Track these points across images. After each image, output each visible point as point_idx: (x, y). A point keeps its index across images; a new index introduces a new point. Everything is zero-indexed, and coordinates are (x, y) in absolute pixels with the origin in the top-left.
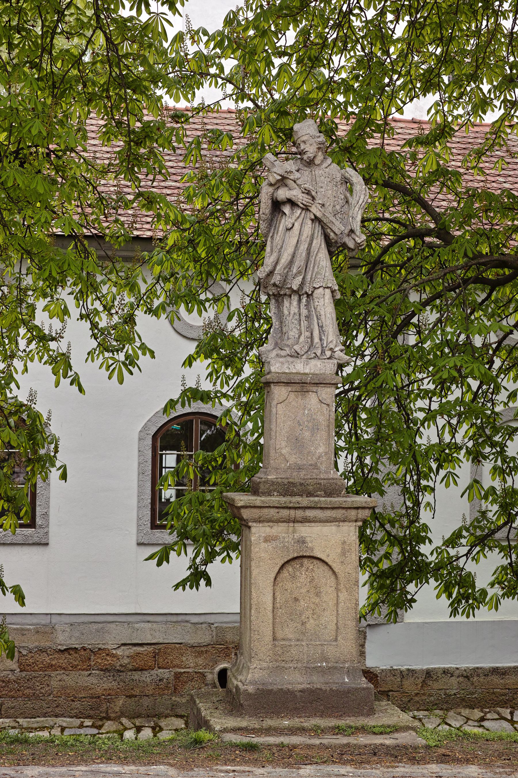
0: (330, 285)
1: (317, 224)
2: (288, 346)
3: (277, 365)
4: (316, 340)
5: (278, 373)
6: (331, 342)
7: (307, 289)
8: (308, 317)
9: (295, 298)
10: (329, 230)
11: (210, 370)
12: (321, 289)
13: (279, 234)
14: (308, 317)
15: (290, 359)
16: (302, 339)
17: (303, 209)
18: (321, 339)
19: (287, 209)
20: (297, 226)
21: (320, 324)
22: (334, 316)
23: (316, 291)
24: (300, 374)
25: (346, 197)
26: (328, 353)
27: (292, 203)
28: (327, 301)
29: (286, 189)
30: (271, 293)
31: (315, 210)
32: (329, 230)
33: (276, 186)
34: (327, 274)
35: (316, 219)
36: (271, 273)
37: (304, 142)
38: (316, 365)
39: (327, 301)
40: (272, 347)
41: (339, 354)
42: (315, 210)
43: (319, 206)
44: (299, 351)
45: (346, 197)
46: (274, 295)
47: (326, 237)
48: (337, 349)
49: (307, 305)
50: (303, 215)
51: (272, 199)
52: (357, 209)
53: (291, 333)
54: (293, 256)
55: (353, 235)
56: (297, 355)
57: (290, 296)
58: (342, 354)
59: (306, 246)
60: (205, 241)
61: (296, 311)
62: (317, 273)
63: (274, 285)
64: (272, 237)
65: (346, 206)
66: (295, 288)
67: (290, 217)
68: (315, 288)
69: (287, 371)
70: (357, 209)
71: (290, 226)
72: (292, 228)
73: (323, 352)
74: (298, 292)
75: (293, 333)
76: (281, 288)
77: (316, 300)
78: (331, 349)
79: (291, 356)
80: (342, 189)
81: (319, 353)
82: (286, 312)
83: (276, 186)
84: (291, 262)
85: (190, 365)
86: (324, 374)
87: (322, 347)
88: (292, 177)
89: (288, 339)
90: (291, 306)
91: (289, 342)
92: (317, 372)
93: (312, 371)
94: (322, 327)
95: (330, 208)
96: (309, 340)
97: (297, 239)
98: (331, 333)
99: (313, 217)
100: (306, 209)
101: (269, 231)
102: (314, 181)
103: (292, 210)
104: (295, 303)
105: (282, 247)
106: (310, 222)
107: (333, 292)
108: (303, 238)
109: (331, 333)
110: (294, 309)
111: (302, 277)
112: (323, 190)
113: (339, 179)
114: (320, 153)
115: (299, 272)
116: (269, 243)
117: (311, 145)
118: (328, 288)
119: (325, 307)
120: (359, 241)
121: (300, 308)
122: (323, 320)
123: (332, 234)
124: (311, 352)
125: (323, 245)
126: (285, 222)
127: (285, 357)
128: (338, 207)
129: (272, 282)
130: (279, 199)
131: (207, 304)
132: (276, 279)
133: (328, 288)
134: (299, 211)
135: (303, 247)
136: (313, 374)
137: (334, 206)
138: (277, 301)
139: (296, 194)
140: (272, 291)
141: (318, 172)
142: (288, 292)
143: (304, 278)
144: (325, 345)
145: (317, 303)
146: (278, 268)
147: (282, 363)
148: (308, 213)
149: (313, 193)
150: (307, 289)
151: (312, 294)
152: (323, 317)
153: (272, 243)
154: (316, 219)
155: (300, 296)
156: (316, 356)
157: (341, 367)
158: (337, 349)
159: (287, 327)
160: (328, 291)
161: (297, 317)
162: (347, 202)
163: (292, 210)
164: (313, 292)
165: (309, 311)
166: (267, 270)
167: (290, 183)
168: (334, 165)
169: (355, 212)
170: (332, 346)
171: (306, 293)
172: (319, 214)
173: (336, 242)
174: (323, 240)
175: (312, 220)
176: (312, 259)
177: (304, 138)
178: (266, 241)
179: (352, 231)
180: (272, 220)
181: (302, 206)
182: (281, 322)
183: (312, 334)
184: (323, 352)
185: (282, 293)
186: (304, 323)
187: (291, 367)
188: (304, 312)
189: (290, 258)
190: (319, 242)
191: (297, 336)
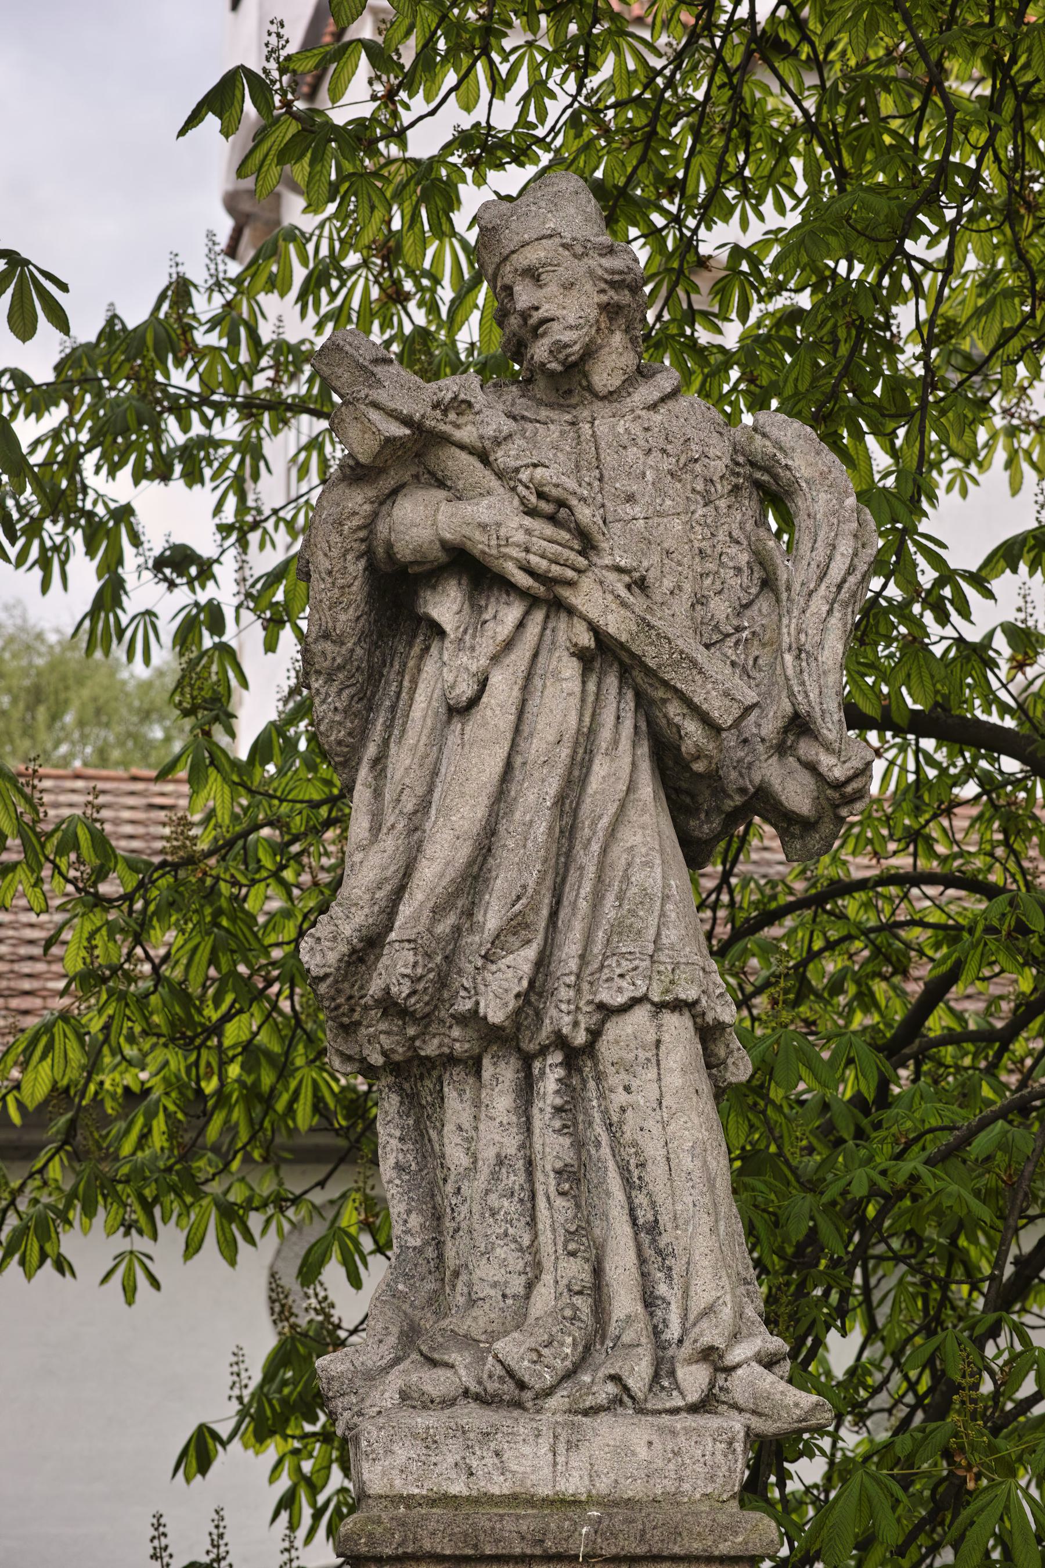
0: (690, 993)
1: (612, 681)
2: (468, 1341)
3: (402, 1453)
4: (624, 1302)
5: (408, 1501)
6: (709, 1311)
7: (562, 1017)
8: (574, 1177)
9: (501, 1075)
10: (674, 709)
11: (284, 1482)
12: (641, 1015)
13: (411, 738)
14: (574, 1177)
15: (474, 1417)
16: (543, 1299)
17: (532, 601)
18: (650, 1301)
19: (445, 606)
20: (503, 686)
21: (644, 1216)
22: (720, 1166)
23: (618, 1030)
24: (530, 1501)
25: (761, 560)
26: (694, 1379)
27: (471, 569)
28: (674, 1080)
29: (442, 494)
30: (376, 1059)
31: (597, 601)
32: (674, 709)
33: (387, 483)
34: (671, 935)
35: (603, 654)
36: (369, 947)
37: (533, 274)
38: (624, 1450)
39: (674, 1080)
40: (385, 1352)
41: (752, 1381)
42: (597, 601)
43: (618, 584)
44: (524, 1368)
45: (761, 560)
46: (394, 1067)
47: (666, 756)
48: (739, 1353)
49: (570, 1110)
50: (533, 629)
51: (369, 553)
52: (818, 605)
53: (486, 1272)
54: (486, 844)
55: (806, 748)
56: (513, 1394)
57: (475, 1066)
58: (773, 1384)
59: (553, 787)
60: (214, 951)
61: (511, 1144)
62: (619, 929)
63: (388, 1006)
64: (379, 762)
65: (764, 604)
66: (496, 1013)
67: (467, 643)
68: (607, 1011)
69: (458, 1488)
70: (818, 605)
71: (465, 689)
72: (474, 702)
73: (663, 1371)
74: (509, 1039)
75: (494, 1270)
76: (425, 1020)
77: (615, 1080)
78: (709, 1355)
79: (485, 1400)
80: (739, 516)
81: (639, 1373)
82: (456, 1156)
83: (387, 483)
84: (474, 878)
85: (204, 1465)
86: (673, 1498)
87: (660, 1344)
88: (466, 434)
89: (472, 1302)
90: (482, 1121)
91: (476, 1323)
92: (633, 1490)
93: (603, 1486)
94: (654, 1228)
95: (681, 605)
96: (584, 1304)
97: (501, 752)
98: (704, 1265)
99: (586, 639)
100: (549, 599)
101: (362, 734)
102: (591, 462)
103: (477, 609)
104: (502, 1102)
105: (424, 805)
106: (571, 668)
107: (708, 1034)
108: (536, 747)
109: (704, 1265)
110: (498, 1136)
111: (531, 953)
112: (637, 510)
113: (719, 467)
114: (618, 339)
115: (516, 927)
116: (361, 795)
117: (568, 286)
118: (678, 1006)
119: (667, 1114)
120: (839, 773)
121: (528, 1128)
122: (660, 1188)
123: (692, 727)
124: (588, 1369)
125: (647, 789)
126: (440, 674)
127: (448, 1403)
128: (720, 608)
129: (375, 987)
130: (404, 551)
131: (255, 1221)
132: (395, 970)
133: (678, 1006)
134: (512, 613)
135: (536, 794)
136: (610, 1503)
137: (700, 600)
138: (411, 1101)
139: (487, 515)
140: (380, 1040)
141: (608, 425)
142: (459, 1040)
143: (542, 962)
144: (674, 1331)
145: (620, 1098)
146: (405, 911)
147: (430, 1441)
148: (562, 623)
149: (585, 514)
150: (562, 1017)
151: (590, 1049)
152: (656, 1172)
153: (378, 794)
154: (603, 654)
155: (527, 1060)
156: (624, 1398)
157: (770, 1454)
158: (739, 1353)
159: (463, 1240)
160: (678, 1028)
161: (515, 1180)
162: (768, 583)
163: (477, 609)
164: (595, 1034)
165: (579, 1145)
166: (347, 930)
167: (461, 465)
168: (690, 399)
169: (811, 622)
170: (711, 1335)
171: (561, 1041)
172: (617, 624)
173: (714, 778)
174: (645, 767)
175: (585, 658)
176: (587, 859)
177: (532, 256)
178: (348, 789)
179: (799, 725)
180: (374, 677)
181: (523, 580)
182: (437, 1217)
183: (598, 1272)
184: (663, 1371)
185: (431, 1048)
186: (554, 1212)
187: (483, 1461)
188: (552, 1147)
189: (464, 852)
190: (620, 768)
191: (517, 1285)
